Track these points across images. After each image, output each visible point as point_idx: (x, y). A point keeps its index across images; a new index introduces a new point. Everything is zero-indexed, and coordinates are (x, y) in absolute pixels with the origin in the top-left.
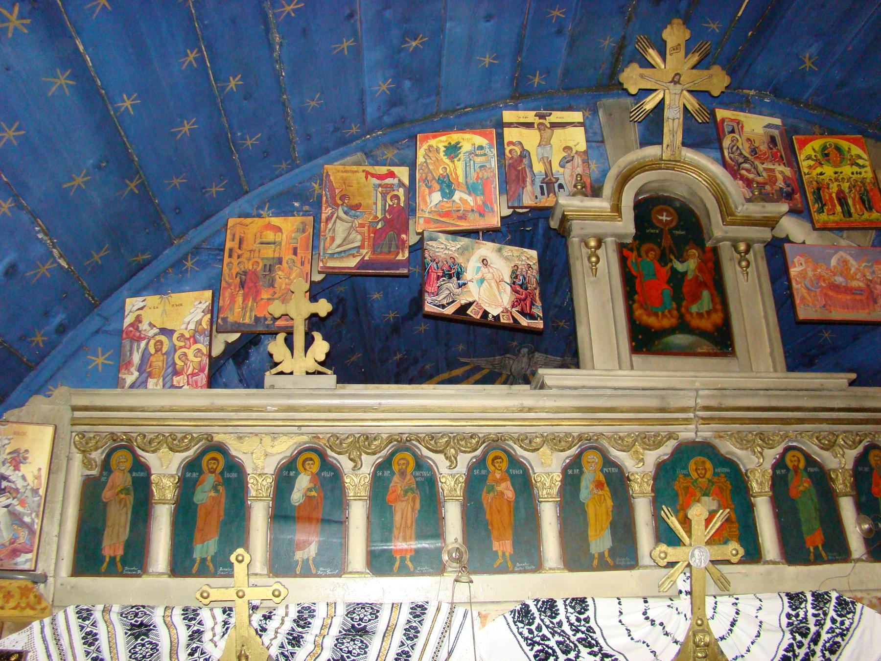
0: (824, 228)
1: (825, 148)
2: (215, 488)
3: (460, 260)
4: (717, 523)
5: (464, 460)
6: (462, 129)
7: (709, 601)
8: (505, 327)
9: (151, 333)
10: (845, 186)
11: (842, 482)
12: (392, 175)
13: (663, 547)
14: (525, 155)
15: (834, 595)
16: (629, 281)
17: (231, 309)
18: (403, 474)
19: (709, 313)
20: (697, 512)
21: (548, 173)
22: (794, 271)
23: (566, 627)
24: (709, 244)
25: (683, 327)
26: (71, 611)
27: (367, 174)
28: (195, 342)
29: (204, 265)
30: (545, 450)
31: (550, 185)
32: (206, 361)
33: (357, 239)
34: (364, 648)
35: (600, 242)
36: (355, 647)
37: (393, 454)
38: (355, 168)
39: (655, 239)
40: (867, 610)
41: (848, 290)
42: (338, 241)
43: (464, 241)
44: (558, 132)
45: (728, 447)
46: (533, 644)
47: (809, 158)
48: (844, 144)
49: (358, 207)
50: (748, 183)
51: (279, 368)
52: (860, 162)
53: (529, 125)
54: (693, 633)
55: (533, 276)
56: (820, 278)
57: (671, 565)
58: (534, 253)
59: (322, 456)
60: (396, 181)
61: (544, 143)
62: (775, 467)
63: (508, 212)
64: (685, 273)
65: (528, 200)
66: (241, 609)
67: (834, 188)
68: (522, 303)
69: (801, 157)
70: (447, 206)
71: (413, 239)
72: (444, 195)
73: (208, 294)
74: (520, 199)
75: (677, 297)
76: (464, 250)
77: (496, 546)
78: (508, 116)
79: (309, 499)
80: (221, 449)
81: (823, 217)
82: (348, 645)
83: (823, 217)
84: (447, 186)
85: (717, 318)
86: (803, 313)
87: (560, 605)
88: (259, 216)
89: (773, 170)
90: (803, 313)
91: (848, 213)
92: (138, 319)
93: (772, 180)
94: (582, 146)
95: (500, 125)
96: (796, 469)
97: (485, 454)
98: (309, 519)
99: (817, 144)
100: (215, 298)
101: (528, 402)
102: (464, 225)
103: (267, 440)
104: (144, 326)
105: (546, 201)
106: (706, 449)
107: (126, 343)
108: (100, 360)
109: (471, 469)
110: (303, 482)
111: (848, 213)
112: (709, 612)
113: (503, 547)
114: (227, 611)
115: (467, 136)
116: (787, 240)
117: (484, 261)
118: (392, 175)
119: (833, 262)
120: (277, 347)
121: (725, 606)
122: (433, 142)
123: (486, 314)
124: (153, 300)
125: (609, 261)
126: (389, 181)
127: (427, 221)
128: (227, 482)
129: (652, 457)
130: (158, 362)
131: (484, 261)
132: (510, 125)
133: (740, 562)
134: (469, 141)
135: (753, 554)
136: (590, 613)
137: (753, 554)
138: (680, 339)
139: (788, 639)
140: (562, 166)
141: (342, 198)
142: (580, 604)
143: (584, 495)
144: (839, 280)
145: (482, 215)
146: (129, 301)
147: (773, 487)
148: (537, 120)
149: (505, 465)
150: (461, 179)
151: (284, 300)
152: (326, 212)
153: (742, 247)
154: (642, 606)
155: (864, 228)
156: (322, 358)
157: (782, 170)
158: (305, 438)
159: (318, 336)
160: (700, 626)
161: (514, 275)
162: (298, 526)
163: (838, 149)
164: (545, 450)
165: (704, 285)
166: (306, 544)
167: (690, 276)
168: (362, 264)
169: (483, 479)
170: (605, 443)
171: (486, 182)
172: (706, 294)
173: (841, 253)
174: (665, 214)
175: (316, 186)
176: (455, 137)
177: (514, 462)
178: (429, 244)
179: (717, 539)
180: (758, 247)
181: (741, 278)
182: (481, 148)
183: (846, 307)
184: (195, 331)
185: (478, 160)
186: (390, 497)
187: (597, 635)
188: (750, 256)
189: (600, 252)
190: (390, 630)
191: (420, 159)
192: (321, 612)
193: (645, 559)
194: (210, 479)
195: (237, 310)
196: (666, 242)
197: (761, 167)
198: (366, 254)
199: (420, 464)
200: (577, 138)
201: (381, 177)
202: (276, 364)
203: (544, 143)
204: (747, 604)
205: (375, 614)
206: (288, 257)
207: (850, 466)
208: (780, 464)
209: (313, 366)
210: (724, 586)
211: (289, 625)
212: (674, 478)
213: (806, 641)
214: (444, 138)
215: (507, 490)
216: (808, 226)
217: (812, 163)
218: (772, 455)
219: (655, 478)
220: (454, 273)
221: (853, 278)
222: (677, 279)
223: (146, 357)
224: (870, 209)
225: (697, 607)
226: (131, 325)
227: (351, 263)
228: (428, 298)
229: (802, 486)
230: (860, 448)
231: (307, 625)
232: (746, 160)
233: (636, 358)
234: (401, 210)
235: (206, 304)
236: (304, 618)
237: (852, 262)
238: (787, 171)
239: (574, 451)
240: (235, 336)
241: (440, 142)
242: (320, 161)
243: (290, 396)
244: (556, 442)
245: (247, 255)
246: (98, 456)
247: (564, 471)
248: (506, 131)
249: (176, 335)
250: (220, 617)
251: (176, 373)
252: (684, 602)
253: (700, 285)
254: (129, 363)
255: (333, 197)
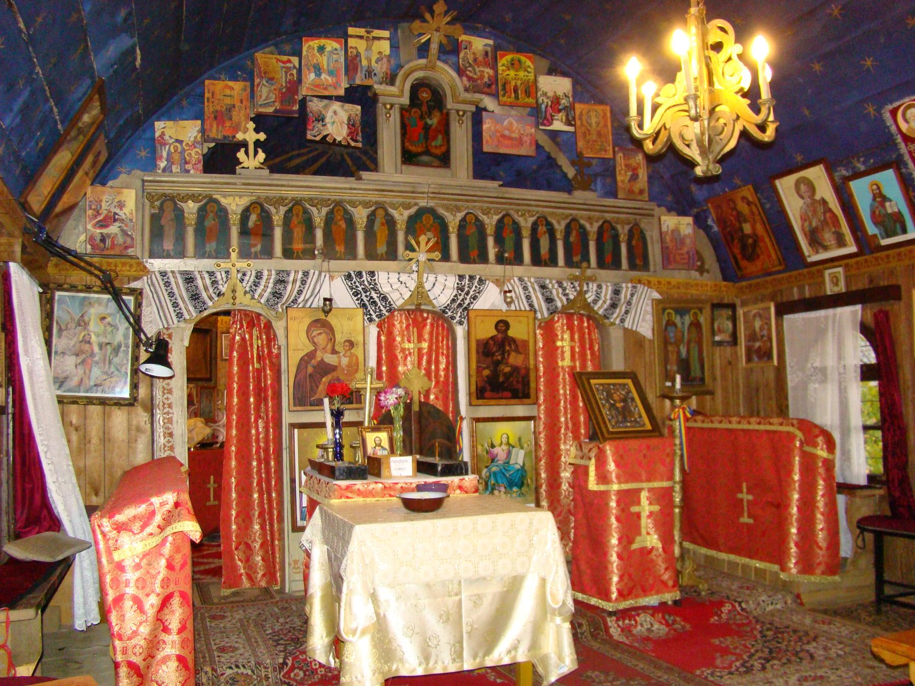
0: (504, 105)
1: (513, 60)
2: (214, 220)
3: (324, 112)
4: (430, 244)
5: (325, 210)
6: (326, 37)
7: (425, 275)
8: (345, 146)
9: (171, 141)
10: (519, 83)
11: (490, 230)
12: (289, 61)
13: (408, 252)
14: (358, 55)
15: (478, 277)
16: (404, 127)
17: (211, 130)
18: (297, 215)
19: (440, 146)
20: (423, 239)
21: (369, 66)
22: (485, 127)
23: (366, 283)
24: (445, 111)
25: (427, 152)
26: (516, 279)
27: (278, 60)
28: (195, 147)
29: (192, 104)
30: (360, 207)
31: (370, 73)
32: (201, 157)
33: (273, 97)
34: (285, 288)
35: (392, 106)
36: (281, 287)
37: (293, 206)
38: (271, 56)
39: (419, 106)
40: (491, 284)
41: (510, 138)
42: (264, 97)
43: (326, 102)
44: (376, 42)
45: (441, 211)
46: (352, 289)
47: (503, 65)
48: (523, 59)
49: (272, 79)
50: (470, 79)
51: (242, 165)
52: (529, 70)
53: (361, 37)
54: (418, 287)
55: (358, 119)
56: (497, 131)
57: (410, 260)
58: (359, 107)
59: (261, 206)
60: (291, 65)
61: (369, 48)
62: (461, 221)
63: (348, 86)
64: (431, 126)
65: (358, 81)
66: (234, 270)
67: (513, 83)
68: (352, 134)
69: (500, 64)
70: (318, 82)
71: (300, 97)
72: (316, 75)
73: (199, 122)
74: (354, 80)
75: (426, 137)
76: (326, 107)
77: (337, 248)
78: (351, 31)
79: (256, 225)
80: (217, 202)
81: (505, 99)
82: (278, 286)
83: (505, 99)
84: (318, 70)
85: (444, 149)
86: (486, 148)
87: (364, 274)
88: (219, 79)
89: (483, 72)
90: (486, 148)
91: (517, 98)
92: (163, 134)
93: (482, 77)
94: (388, 52)
95: (346, 36)
96: (470, 223)
97: (333, 208)
98: (256, 234)
99: (509, 57)
100: (203, 124)
101: (354, 186)
102: (326, 93)
103: (237, 199)
104: (166, 137)
105: (367, 82)
106: (431, 211)
107: (158, 145)
108: (143, 154)
109: (327, 214)
110: (253, 218)
111: (517, 98)
112: (425, 280)
113: (340, 248)
114: (227, 272)
115: (329, 42)
116: (485, 109)
117: (335, 113)
118: (289, 61)
119: (505, 123)
120: (241, 155)
121: (432, 278)
122: (311, 43)
123: (335, 140)
124: (169, 124)
125: (395, 116)
126: (289, 65)
127: (308, 88)
128: (219, 217)
129: (407, 213)
130: (176, 157)
131: (335, 113)
132: (352, 36)
133: (439, 261)
134: (331, 45)
135: (446, 257)
136: (376, 277)
137: (446, 257)
138: (425, 158)
139: (455, 292)
140: (377, 63)
141: (265, 73)
142: (372, 274)
143: (376, 228)
144: (507, 133)
145: (335, 88)
146: (156, 123)
147: (458, 230)
148: (365, 35)
149: (342, 213)
150: (325, 67)
151: (245, 132)
152: (257, 81)
153: (461, 113)
154: (397, 275)
155: (524, 106)
156: (262, 161)
157: (488, 71)
158: (254, 198)
159: (260, 151)
160: (420, 285)
161: (349, 120)
162: (252, 237)
163: (519, 61)
164: (360, 207)
165: (440, 132)
166: (256, 245)
167: (434, 127)
168: (276, 111)
169: (332, 219)
170: (387, 206)
171: (338, 70)
172: (440, 137)
173: (510, 119)
174: (634, 509)
175: (249, 63)
176: (323, 42)
177: (346, 211)
178: (310, 104)
179: (430, 250)
180: (469, 114)
181: (458, 129)
182: (336, 49)
183: (507, 147)
184: (194, 141)
185: (335, 57)
186: (292, 225)
187: (379, 286)
188: (464, 118)
189: (391, 112)
190: (294, 281)
191: (304, 53)
192: (266, 273)
193: (400, 257)
194: (211, 215)
195: (214, 131)
196: (424, 109)
197: (477, 69)
198: (278, 106)
199: (306, 211)
200: (385, 47)
201: (284, 62)
202: (241, 163)
203: (369, 48)
204: (441, 278)
205: (288, 275)
206: (238, 104)
207: (494, 223)
208: (463, 219)
209: (258, 165)
210: (432, 271)
211: (252, 278)
212: (416, 223)
213: (463, 294)
214: (317, 41)
215: (343, 224)
216: (497, 103)
217: (504, 68)
218: (460, 216)
219: (407, 222)
220: (321, 119)
221: (514, 132)
222: (427, 128)
223: (169, 154)
224: (528, 97)
225: (420, 277)
226: (160, 136)
227: (270, 110)
228: (308, 132)
229: (472, 231)
230: (500, 215)
231: (261, 278)
232: (470, 65)
233: (404, 167)
234: (295, 82)
235: (198, 128)
236: (259, 276)
237: (515, 123)
238: (491, 72)
239: (373, 208)
240: (212, 145)
241: (315, 43)
242: (252, 51)
243: (248, 179)
244: (366, 205)
245: (216, 102)
246: (157, 203)
247: (368, 217)
248: (350, 40)
249: (184, 144)
250: (224, 275)
251: (186, 163)
252: (415, 276)
253: (437, 131)
254: (161, 157)
255: (260, 72)
